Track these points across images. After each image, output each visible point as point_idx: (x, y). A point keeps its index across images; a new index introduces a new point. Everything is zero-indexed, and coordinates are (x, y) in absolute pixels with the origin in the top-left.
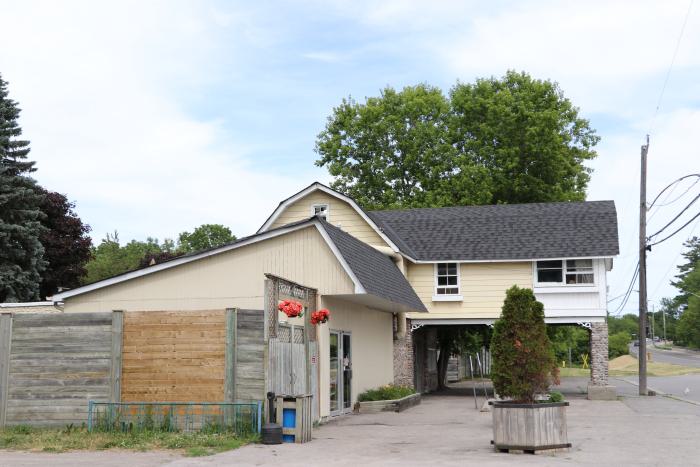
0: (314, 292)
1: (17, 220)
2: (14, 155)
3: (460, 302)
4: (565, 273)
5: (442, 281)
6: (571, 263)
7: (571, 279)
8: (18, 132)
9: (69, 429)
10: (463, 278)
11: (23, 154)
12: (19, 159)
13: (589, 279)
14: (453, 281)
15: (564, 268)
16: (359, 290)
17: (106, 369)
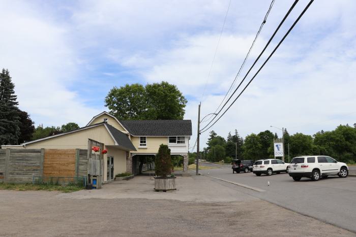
0: (103, 144)
1: (12, 119)
2: (12, 99)
3: (146, 148)
4: (177, 140)
5: (141, 142)
6: (178, 137)
7: (178, 142)
8: (13, 93)
9: (27, 184)
10: (148, 141)
11: (15, 99)
12: (13, 101)
13: (183, 142)
14: (145, 142)
15: (177, 139)
16: (117, 144)
17: (38, 166)
